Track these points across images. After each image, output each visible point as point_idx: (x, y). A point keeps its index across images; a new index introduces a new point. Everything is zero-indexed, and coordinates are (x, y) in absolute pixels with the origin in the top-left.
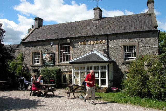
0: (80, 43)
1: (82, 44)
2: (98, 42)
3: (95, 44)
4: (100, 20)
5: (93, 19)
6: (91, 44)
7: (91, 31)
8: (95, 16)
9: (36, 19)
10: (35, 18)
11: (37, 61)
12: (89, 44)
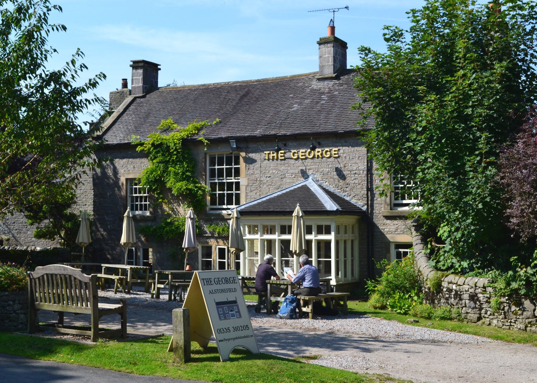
0: (269, 154)
1: (273, 157)
2: (318, 152)
3: (312, 159)
4: (337, 78)
5: (314, 73)
6: (298, 158)
7: (292, 117)
8: (322, 67)
9: (137, 65)
10: (134, 62)
11: (141, 205)
12: (292, 158)
